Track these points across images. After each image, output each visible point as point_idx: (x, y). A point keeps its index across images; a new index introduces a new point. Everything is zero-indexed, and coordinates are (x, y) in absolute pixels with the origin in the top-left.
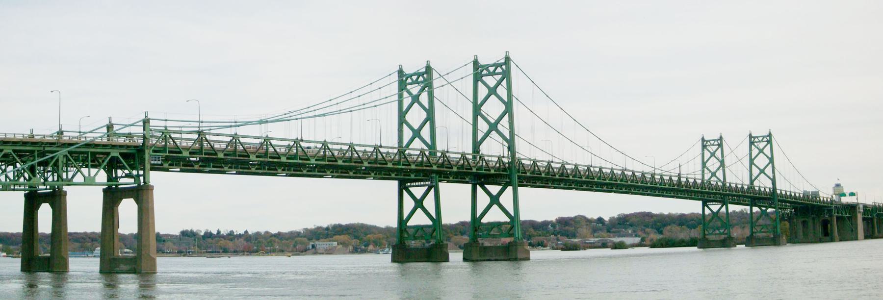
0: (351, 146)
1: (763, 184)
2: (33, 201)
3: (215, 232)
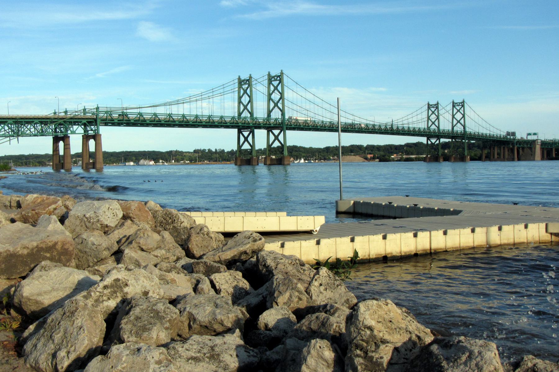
0: (183, 116)
1: (459, 128)
2: (56, 140)
3: (214, 150)
